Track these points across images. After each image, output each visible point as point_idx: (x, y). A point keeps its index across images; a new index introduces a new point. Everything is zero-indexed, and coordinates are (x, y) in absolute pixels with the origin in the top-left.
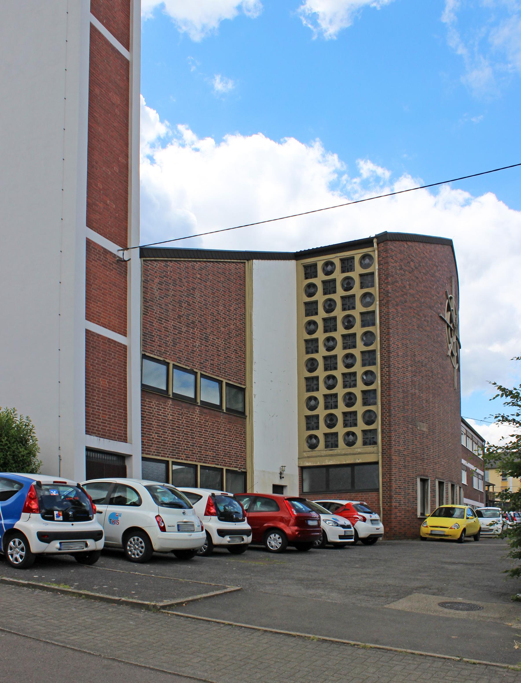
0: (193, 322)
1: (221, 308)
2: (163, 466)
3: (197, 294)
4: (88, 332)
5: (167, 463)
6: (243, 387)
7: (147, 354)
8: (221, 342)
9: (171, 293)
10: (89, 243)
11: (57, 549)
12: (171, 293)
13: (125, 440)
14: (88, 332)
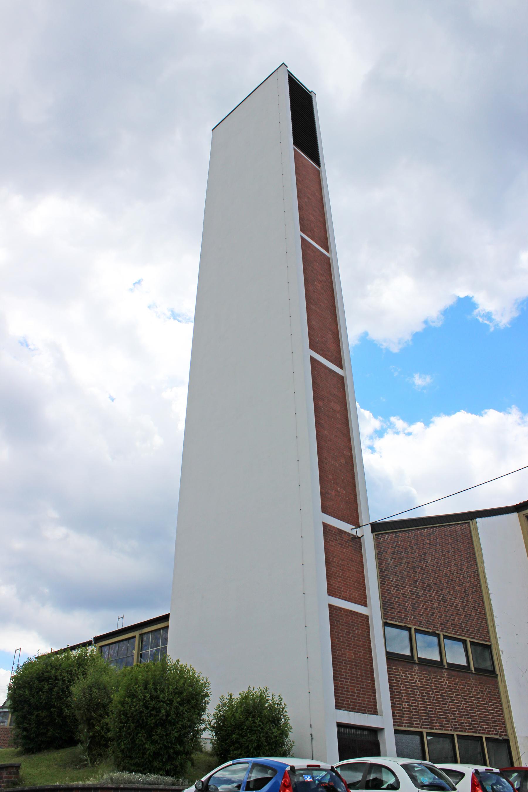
0: (429, 585)
1: (453, 568)
2: (417, 738)
7: (389, 621)
8: (459, 601)
12: (404, 561)
13: (375, 713)
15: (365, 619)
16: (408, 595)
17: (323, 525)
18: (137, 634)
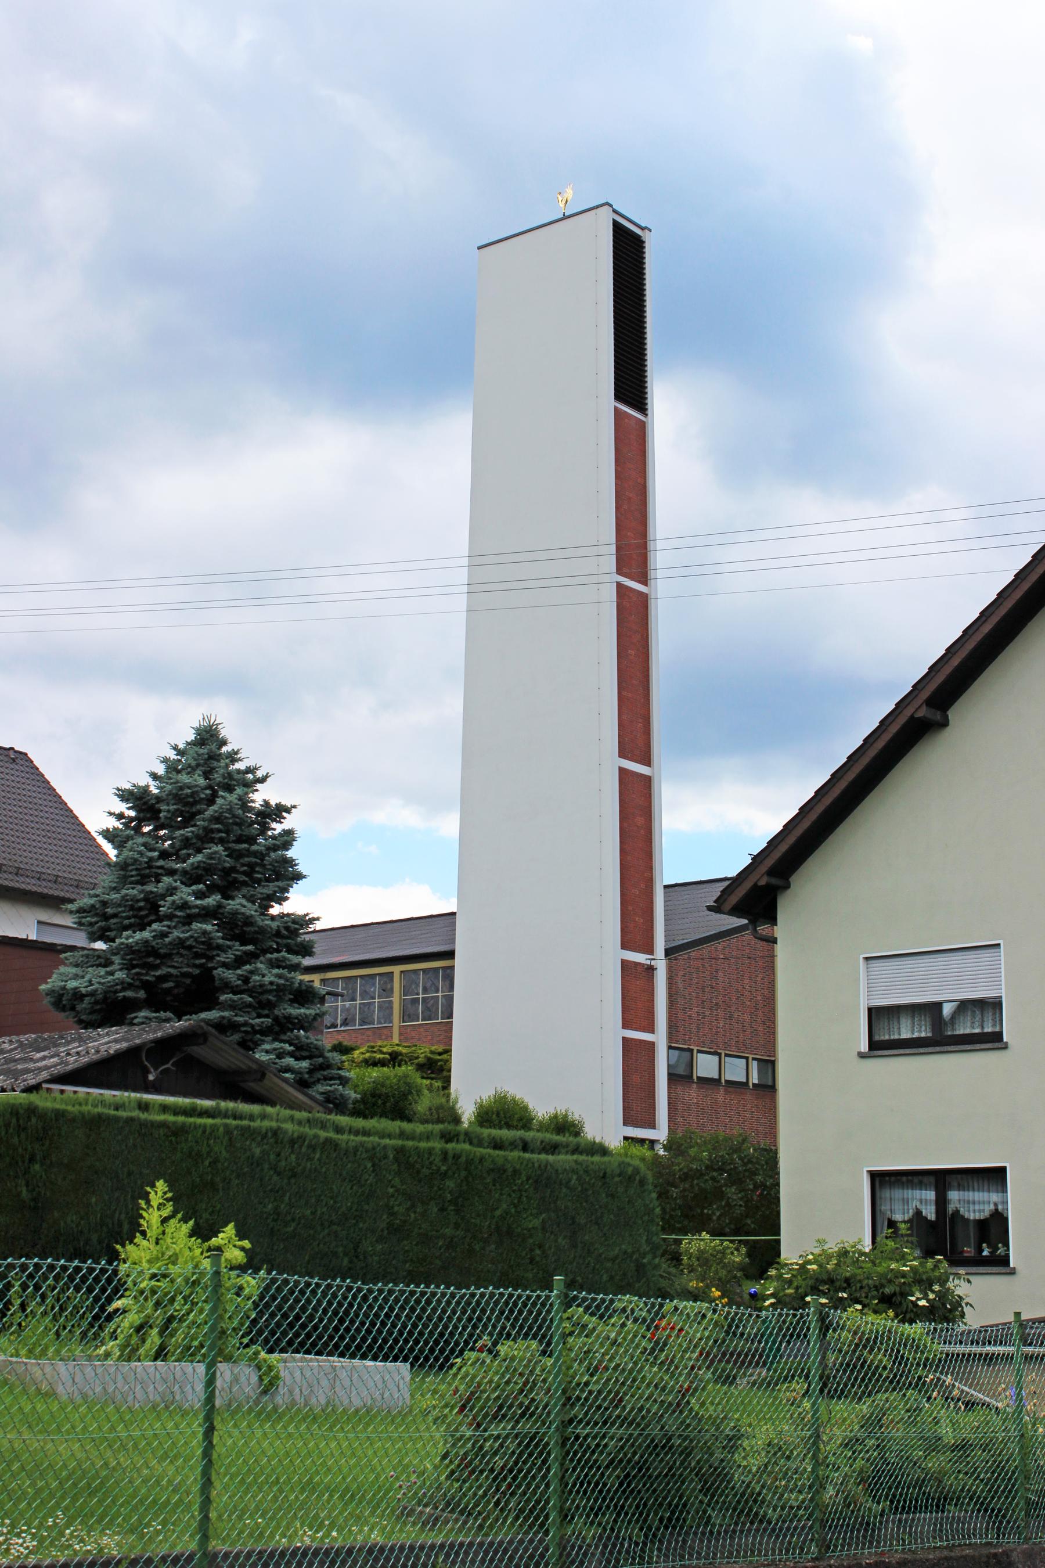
0: (717, 1004)
1: (746, 981)
2: (744, 1061)
3: (720, 974)
4: (622, 771)
5: (747, 1058)
6: (773, 1059)
7: (673, 1045)
8: (747, 1017)
9: (695, 981)
10: (614, 221)
11: (175, 748)
12: (695, 981)
13: (654, 1127)
14: (622, 771)
15: (651, 1046)
16: (695, 1015)
17: (614, 225)
18: (397, 969)
